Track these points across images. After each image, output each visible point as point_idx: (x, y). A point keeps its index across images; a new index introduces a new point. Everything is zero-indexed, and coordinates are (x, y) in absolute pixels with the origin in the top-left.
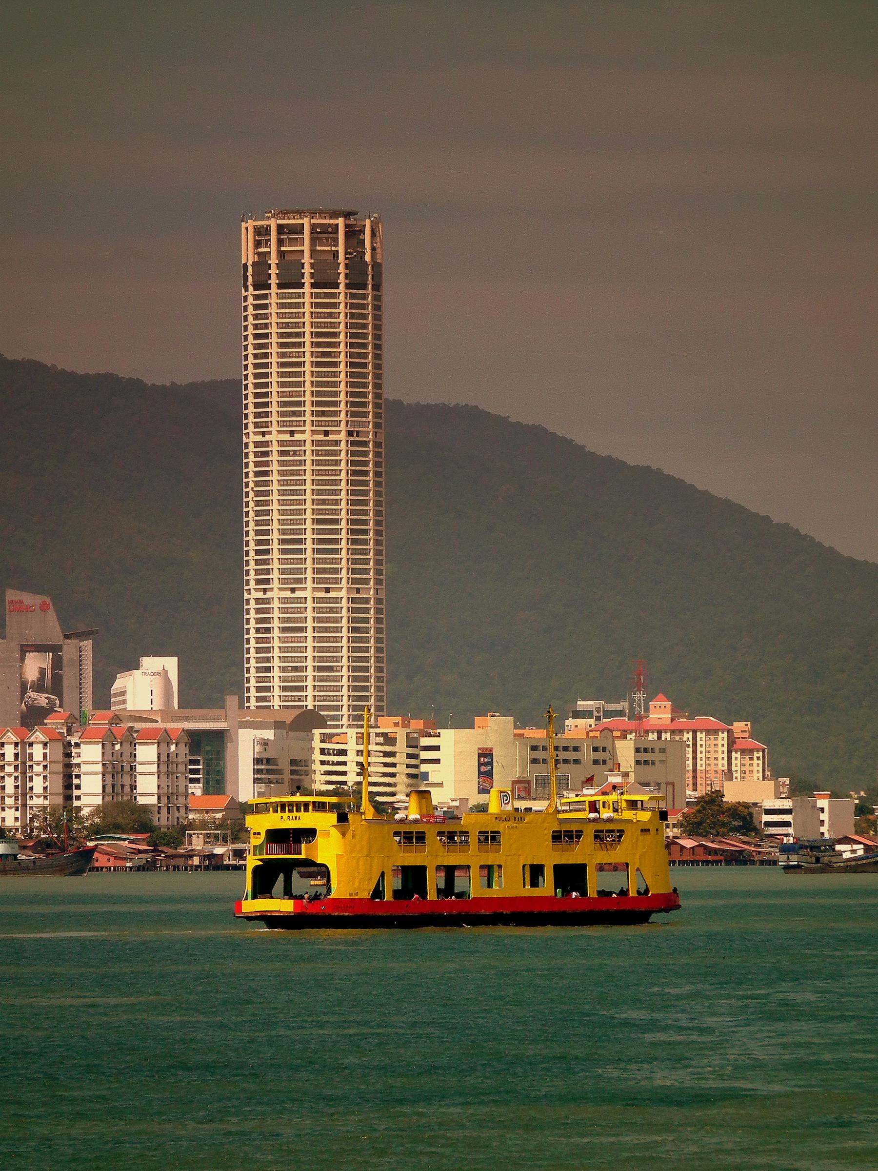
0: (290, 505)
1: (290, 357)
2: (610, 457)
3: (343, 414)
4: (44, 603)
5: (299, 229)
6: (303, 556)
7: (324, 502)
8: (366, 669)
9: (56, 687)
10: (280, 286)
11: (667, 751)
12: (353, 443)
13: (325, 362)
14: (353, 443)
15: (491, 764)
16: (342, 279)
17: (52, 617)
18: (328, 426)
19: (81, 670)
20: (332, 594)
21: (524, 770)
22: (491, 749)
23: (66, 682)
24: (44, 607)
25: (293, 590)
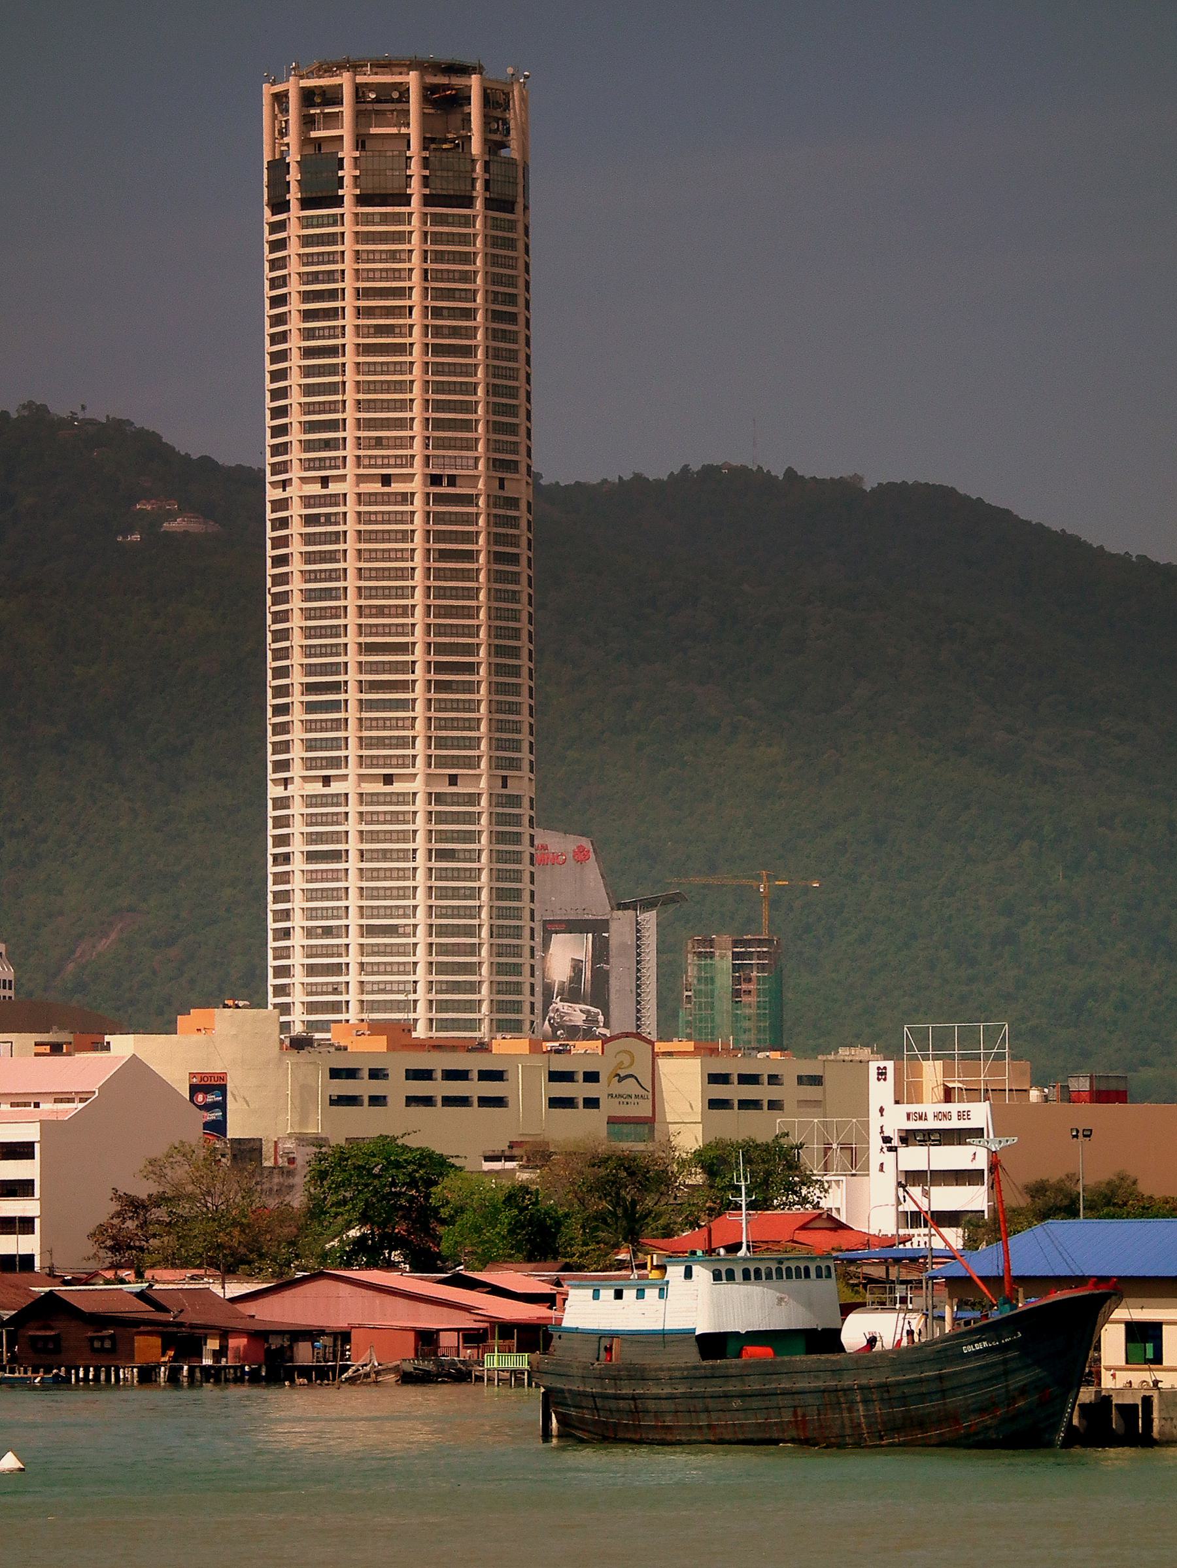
0: (321, 618)
1: (319, 338)
2: (638, 477)
3: (418, 443)
4: (581, 849)
5: (332, 97)
6: (341, 715)
7: (381, 611)
8: (470, 931)
9: (599, 995)
10: (305, 204)
11: (827, 1081)
12: (440, 499)
13: (383, 345)
14: (440, 499)
15: (222, 1106)
16: (415, 189)
17: (592, 872)
18: (389, 466)
19: (638, 962)
20: (397, 787)
21: (304, 1119)
22: (223, 1076)
23: (614, 983)
24: (580, 856)
25: (326, 781)
